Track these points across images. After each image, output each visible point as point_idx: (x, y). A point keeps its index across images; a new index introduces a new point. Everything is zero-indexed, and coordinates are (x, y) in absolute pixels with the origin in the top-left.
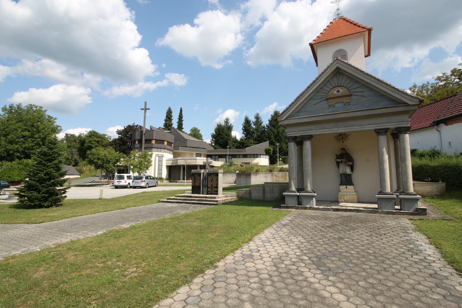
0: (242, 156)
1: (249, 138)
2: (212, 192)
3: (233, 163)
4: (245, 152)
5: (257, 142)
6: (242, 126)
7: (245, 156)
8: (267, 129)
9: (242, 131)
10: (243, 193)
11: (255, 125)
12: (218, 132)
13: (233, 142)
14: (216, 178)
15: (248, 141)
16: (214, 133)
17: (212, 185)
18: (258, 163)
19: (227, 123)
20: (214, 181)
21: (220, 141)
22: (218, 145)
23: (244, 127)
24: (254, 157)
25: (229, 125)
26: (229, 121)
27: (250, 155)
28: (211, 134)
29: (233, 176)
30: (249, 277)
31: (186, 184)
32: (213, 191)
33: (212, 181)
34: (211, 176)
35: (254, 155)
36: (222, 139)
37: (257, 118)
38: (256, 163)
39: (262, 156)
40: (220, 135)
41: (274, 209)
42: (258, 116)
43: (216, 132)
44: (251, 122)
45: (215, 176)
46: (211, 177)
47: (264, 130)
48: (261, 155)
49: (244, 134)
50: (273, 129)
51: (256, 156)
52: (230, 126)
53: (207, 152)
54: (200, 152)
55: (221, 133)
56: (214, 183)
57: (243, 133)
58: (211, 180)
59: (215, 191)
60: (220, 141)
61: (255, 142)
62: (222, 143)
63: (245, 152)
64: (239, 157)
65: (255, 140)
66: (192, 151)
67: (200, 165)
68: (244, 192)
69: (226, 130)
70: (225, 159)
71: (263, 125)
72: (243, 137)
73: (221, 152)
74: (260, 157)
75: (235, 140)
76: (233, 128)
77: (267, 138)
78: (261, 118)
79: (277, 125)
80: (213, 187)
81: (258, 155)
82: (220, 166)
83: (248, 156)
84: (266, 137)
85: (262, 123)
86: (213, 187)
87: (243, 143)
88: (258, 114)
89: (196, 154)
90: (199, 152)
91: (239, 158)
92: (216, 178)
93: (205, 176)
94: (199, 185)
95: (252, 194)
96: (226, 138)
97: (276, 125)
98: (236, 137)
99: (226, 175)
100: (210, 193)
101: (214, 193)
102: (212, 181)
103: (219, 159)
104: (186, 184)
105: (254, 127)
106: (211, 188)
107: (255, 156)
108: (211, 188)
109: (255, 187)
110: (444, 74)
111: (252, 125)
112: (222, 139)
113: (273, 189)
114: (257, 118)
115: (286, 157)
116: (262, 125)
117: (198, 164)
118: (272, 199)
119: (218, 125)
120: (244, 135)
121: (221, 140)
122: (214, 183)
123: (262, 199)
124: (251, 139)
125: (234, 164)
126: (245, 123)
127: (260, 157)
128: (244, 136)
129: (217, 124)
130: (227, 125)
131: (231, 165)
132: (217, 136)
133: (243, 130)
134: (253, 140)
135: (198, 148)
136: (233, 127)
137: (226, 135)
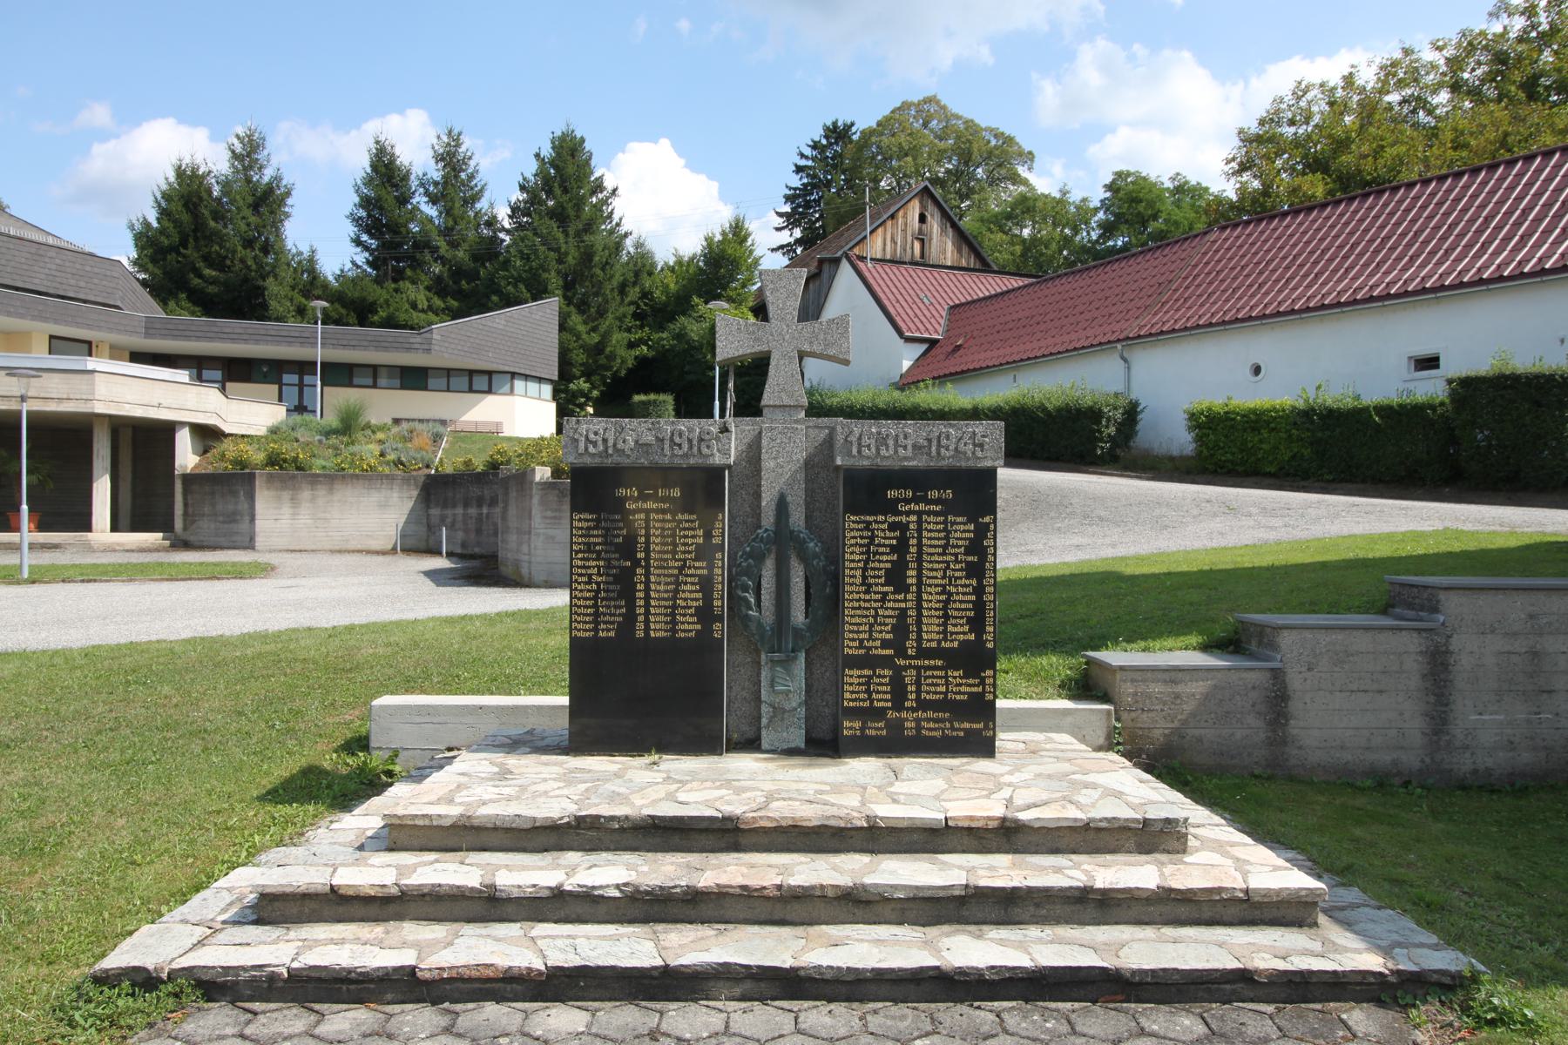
0: (390, 377)
1: (398, 276)
2: (897, 726)
3: (362, 421)
4: (428, 351)
5: (455, 304)
6: (357, 200)
7: (414, 378)
8: (508, 232)
9: (350, 229)
10: (1188, 707)
11: (433, 200)
12: (185, 217)
13: (293, 288)
14: (963, 530)
15: (397, 290)
16: (155, 224)
17: (901, 629)
18: (498, 424)
19: (246, 169)
20: (935, 578)
21: (200, 276)
22: (189, 298)
23: (365, 202)
24: (471, 390)
25: (266, 179)
26: (261, 156)
27: (449, 372)
28: (132, 227)
29: (383, 506)
30: (311, 1036)
31: (29, 560)
32: (923, 705)
33: (896, 577)
34: (891, 507)
35: (471, 373)
36: (211, 266)
37: (451, 160)
38: (485, 423)
39: (519, 384)
40: (196, 239)
41: (220, 633)
42: (458, 145)
43: (164, 213)
44: (414, 183)
45: (949, 508)
46: (881, 522)
47: (494, 240)
48: (514, 375)
49: (366, 248)
50: (560, 236)
51: (481, 380)
52: (270, 190)
53: (148, 335)
54: (89, 327)
55: (212, 224)
56: (932, 598)
57: (357, 242)
58: (886, 560)
59: (944, 705)
60: (200, 276)
61: (438, 302)
62: (212, 289)
63: (428, 351)
64: (370, 381)
65: (438, 287)
66: (22, 316)
67: (110, 417)
68: (1198, 688)
69: (247, 212)
70: (276, 387)
71: (482, 205)
72: (353, 263)
73: (257, 342)
74: (507, 388)
75: (309, 281)
76: (289, 201)
77: (522, 286)
78: (472, 163)
79: (578, 217)
80: (923, 653)
81: (495, 377)
82: (262, 431)
83: (431, 382)
84: (518, 280)
85: (476, 197)
86: (923, 653)
87: (364, 299)
88: (455, 139)
89: (51, 337)
90: (78, 325)
91: (375, 386)
92: (963, 530)
93: (782, 505)
94: (689, 627)
95: (1295, 706)
96: (242, 261)
97: (572, 213)
98: (312, 261)
99: (337, 496)
100: (876, 729)
101: (931, 730)
102: (896, 577)
103: (228, 385)
104: (29, 560)
105: (431, 211)
106: (885, 662)
107: (479, 382)
108: (885, 662)
109: (1340, 636)
110: (1407, 52)
111: (420, 200)
112: (219, 263)
113: (1534, 654)
114: (451, 160)
115: (652, 397)
116: (478, 206)
117: (100, 408)
118: (1526, 757)
119: (180, 173)
120: (361, 258)
121: (207, 272)
122: (932, 598)
123: (1412, 760)
124: (413, 282)
125: (368, 426)
126: (368, 181)
127: (512, 392)
128: (368, 262)
129: (175, 161)
130: (248, 180)
131: (348, 426)
132: (176, 239)
133: (356, 221)
134: (428, 288)
135: (85, 301)
136: (288, 194)
137: (249, 243)
